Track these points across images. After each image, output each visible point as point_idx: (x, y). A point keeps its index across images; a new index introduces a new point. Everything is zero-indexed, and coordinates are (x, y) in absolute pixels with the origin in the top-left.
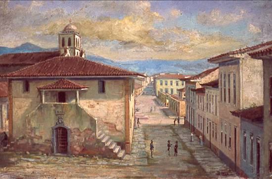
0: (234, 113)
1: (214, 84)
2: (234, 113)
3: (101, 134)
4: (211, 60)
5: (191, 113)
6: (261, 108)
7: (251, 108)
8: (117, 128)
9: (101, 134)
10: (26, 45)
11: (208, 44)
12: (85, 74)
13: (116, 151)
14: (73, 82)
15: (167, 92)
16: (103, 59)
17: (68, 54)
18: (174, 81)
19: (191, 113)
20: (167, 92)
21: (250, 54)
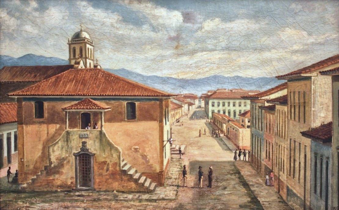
0: (304, 134)
1: (283, 101)
2: (304, 134)
3: (125, 164)
4: (279, 78)
5: (256, 145)
6: (330, 124)
7: (281, 97)
8: (202, 106)
9: (125, 164)
10: (28, 56)
11: (295, 58)
12: (92, 95)
13: (147, 184)
14: (94, 101)
15: (224, 113)
16: (129, 73)
17: (81, 66)
18: (237, 102)
19: (256, 145)
20: (224, 113)
21: (320, 72)
